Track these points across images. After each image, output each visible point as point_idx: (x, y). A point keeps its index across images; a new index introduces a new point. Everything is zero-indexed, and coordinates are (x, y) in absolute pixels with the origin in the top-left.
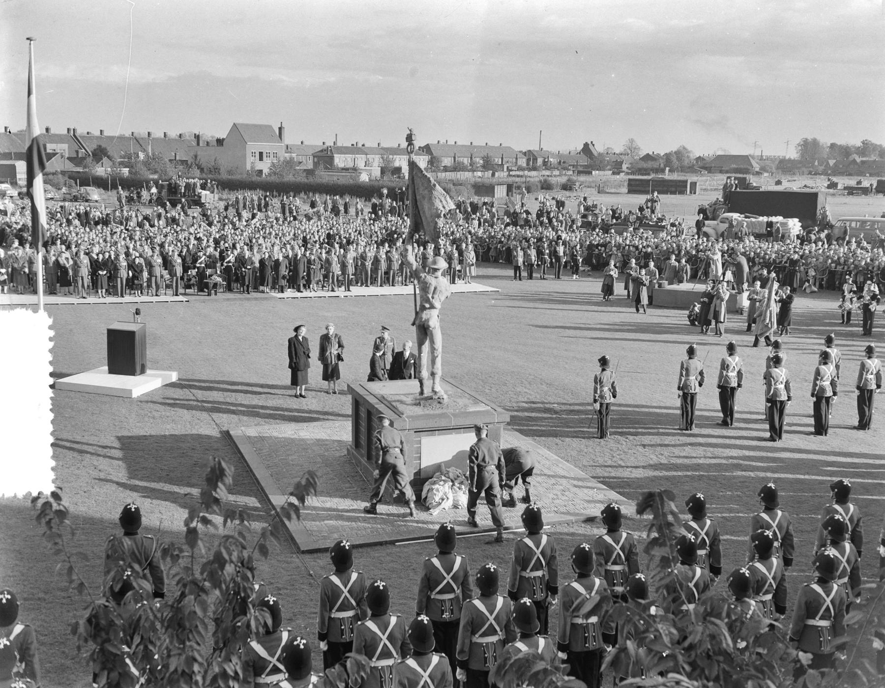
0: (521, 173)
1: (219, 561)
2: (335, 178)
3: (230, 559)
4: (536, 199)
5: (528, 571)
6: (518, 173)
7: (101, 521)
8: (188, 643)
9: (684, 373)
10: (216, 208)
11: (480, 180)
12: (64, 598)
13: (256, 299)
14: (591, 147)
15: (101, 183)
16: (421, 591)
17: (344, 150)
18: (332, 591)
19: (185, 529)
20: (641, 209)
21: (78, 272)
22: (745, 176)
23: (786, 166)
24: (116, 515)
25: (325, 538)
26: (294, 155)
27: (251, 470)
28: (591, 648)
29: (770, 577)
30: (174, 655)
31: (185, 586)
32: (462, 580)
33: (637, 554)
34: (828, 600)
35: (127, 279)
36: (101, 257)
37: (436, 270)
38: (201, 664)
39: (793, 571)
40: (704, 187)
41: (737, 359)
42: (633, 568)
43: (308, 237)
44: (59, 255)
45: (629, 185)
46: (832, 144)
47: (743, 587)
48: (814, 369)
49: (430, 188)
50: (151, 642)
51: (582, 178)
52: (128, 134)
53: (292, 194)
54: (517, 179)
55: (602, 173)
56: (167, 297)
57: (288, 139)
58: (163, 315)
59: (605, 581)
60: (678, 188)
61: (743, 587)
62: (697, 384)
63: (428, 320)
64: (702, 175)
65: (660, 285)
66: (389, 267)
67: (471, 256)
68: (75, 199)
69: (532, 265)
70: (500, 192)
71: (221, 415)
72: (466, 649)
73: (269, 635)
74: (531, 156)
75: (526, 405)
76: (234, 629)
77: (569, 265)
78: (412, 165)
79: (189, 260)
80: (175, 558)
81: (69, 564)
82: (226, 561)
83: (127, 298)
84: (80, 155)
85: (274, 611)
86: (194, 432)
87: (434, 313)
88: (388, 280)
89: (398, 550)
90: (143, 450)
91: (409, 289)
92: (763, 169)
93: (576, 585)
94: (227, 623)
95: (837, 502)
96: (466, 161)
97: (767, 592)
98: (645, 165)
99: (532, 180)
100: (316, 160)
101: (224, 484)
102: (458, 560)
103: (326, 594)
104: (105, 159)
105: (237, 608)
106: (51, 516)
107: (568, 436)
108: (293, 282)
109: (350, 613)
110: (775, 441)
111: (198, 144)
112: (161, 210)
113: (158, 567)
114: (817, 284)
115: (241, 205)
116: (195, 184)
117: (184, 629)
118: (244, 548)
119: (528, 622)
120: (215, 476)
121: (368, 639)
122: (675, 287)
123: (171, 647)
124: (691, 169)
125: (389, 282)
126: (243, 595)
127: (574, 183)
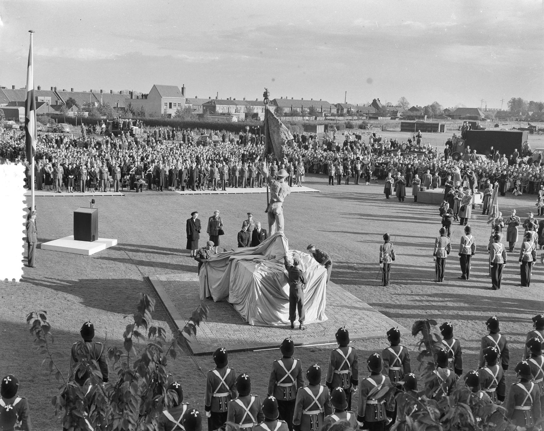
0: (333, 118)
1: (145, 360)
2: (217, 120)
3: (152, 359)
4: (343, 134)
5: (339, 370)
6: (331, 118)
7: (69, 333)
8: (125, 411)
9: (438, 245)
10: (142, 137)
11: (307, 122)
12: (45, 380)
13: (167, 194)
14: (377, 102)
15: (71, 121)
16: (271, 381)
17: (222, 102)
18: (215, 380)
19: (124, 340)
20: (410, 141)
21: (56, 176)
22: (475, 121)
23: (501, 116)
24: (78, 329)
25: (209, 346)
26: (191, 105)
27: (162, 302)
28: (379, 420)
29: (495, 377)
30: (116, 419)
31: (123, 375)
32: (297, 374)
33: (409, 360)
34: (529, 393)
35: (87, 181)
36: (70, 167)
37: (281, 178)
38: (133, 425)
39: (508, 373)
40: (449, 128)
41: (471, 237)
42: (407, 369)
43: (199, 156)
44: (45, 166)
45: (402, 126)
46: (531, 102)
47: (474, 382)
48: (521, 244)
49: (279, 126)
50: (102, 410)
51: (372, 121)
52: (88, 91)
53: (189, 129)
54: (331, 122)
55: (384, 118)
56: (111, 192)
57: (188, 94)
58: (109, 204)
59: (388, 378)
60: (433, 128)
61: (474, 382)
62: (446, 252)
63: (276, 209)
64: (448, 121)
65: (422, 189)
66: (250, 176)
67: (302, 169)
68: (55, 131)
69: (340, 175)
70: (320, 130)
71: (144, 267)
72: (299, 418)
73: (175, 407)
74: (339, 107)
75: (337, 264)
76: (154, 403)
77: (364, 176)
78: (267, 112)
79: (125, 170)
80: (117, 357)
81: (50, 360)
82: (150, 360)
83: (86, 193)
84: (58, 104)
85: (179, 391)
86: (127, 277)
87: (280, 205)
88: (249, 184)
89: (255, 354)
90: (95, 288)
91: (264, 190)
92: (487, 117)
93: (370, 379)
94: (150, 399)
95: (537, 329)
96: (299, 110)
97: (492, 387)
98: (411, 114)
99: (340, 122)
100: (204, 108)
101: (149, 311)
102: (295, 362)
103: (210, 382)
104: (74, 107)
105: (156, 389)
106: (40, 329)
107: (363, 284)
108: (190, 184)
109: (226, 394)
110: (496, 289)
111: (132, 98)
112: (108, 138)
113: (105, 363)
114: (522, 190)
115: (158, 135)
116: (129, 123)
117: (123, 402)
118: (161, 351)
119: (340, 402)
120: (144, 305)
121: (238, 410)
122: (430, 190)
123: (114, 413)
124: (441, 117)
125: (250, 185)
126: (160, 382)
127: (367, 125)
